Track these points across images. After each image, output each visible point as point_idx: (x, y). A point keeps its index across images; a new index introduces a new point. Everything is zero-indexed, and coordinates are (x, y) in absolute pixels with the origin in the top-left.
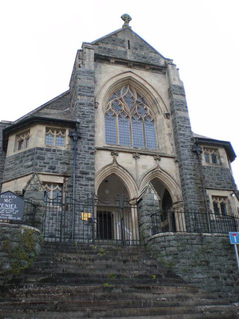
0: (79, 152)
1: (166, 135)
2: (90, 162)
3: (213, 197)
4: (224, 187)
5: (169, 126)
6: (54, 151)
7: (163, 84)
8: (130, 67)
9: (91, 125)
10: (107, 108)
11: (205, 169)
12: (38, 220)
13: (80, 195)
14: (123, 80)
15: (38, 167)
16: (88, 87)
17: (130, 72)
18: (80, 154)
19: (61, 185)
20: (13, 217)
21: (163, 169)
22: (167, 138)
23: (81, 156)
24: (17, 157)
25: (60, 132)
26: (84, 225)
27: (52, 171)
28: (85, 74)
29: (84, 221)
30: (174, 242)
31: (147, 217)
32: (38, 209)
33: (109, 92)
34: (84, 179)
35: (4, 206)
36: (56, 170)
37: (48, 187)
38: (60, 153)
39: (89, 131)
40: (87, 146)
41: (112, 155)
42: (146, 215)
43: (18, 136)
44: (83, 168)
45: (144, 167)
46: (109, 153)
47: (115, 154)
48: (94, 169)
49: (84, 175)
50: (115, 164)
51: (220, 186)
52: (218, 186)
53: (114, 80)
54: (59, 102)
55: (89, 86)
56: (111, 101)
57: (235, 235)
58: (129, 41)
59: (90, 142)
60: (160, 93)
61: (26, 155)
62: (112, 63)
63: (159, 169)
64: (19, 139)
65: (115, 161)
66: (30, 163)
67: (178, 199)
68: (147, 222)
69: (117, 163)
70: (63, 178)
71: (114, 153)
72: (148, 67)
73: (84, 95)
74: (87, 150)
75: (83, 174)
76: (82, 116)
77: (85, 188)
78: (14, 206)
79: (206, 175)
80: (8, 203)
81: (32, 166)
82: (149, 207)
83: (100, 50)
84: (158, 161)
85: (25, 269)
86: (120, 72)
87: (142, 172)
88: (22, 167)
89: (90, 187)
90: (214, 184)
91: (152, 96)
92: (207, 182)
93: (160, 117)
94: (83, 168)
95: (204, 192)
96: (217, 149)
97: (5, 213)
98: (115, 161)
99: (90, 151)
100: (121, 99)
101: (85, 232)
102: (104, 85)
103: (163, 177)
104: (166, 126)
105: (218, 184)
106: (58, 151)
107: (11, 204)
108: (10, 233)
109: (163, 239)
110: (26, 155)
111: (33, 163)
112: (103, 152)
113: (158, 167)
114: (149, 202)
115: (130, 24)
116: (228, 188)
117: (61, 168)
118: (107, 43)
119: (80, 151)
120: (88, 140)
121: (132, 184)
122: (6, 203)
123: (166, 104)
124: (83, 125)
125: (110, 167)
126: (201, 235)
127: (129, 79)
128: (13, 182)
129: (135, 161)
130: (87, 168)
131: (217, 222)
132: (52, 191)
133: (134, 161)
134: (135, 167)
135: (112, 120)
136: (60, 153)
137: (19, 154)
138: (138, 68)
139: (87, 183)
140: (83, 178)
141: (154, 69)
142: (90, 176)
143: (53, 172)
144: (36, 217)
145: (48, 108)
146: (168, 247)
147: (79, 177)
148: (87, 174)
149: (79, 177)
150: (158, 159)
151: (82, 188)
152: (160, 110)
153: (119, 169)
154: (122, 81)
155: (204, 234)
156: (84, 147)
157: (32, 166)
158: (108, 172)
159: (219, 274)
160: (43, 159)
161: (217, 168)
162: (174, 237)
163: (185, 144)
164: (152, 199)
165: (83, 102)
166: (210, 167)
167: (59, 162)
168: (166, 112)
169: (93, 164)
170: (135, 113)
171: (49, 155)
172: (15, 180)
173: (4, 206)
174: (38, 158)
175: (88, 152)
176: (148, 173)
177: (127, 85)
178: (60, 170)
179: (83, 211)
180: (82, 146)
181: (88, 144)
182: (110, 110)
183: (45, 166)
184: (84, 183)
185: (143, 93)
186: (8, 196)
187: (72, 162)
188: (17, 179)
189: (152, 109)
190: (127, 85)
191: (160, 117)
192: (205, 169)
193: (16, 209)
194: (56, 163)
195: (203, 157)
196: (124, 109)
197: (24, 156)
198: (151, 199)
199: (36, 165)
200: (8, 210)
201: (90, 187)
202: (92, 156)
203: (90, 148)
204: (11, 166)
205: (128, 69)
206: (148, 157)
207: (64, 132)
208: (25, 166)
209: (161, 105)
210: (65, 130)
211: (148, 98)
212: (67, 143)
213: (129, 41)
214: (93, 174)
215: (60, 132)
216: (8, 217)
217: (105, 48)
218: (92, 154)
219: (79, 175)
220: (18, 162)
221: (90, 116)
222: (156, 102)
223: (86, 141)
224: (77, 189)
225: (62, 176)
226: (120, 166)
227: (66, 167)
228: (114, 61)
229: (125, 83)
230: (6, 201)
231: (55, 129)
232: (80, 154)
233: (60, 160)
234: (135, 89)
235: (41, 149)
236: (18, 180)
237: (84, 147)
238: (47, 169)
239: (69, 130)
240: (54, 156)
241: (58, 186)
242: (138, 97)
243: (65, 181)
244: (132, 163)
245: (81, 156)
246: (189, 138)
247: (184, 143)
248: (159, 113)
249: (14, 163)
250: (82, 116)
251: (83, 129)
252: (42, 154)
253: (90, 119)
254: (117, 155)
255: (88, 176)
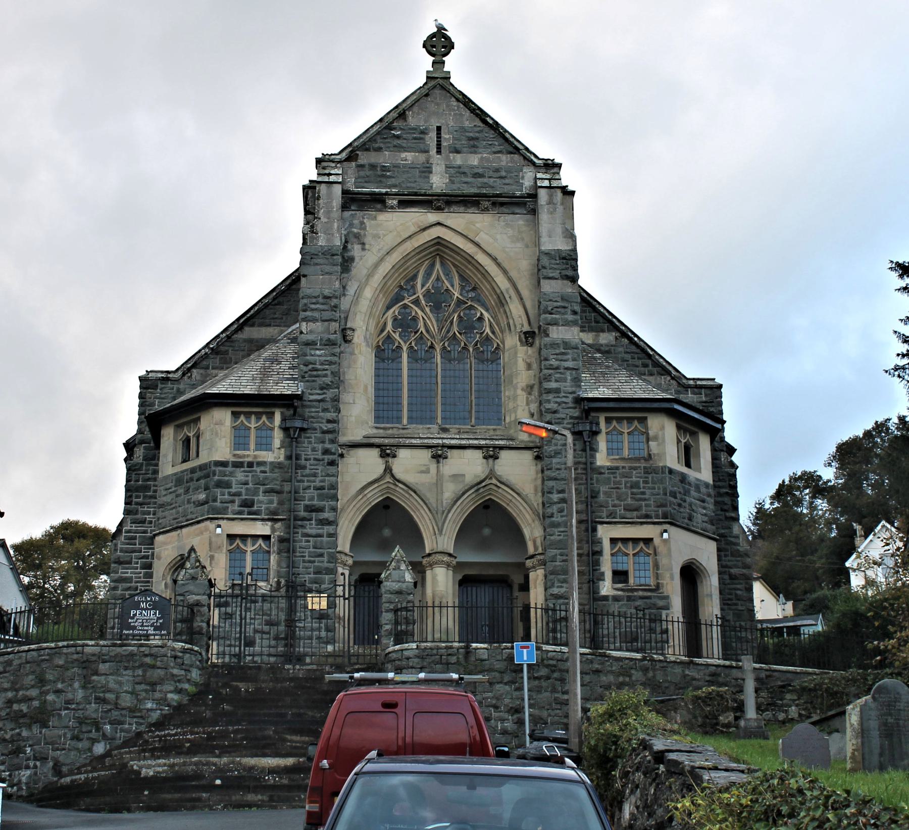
0: (303, 462)
1: (519, 392)
2: (326, 484)
3: (613, 541)
4: (647, 516)
5: (529, 367)
6: (250, 465)
7: (527, 246)
8: (439, 209)
9: (330, 394)
10: (382, 331)
11: (601, 473)
12: (198, 629)
13: (304, 556)
14: (420, 250)
15: (218, 504)
16: (326, 297)
17: (439, 224)
18: (304, 467)
19: (266, 538)
20: (154, 630)
21: (504, 480)
22: (522, 396)
23: (307, 471)
24: (179, 480)
25: (264, 418)
26: (312, 619)
27: (246, 509)
28: (319, 261)
29: (312, 610)
30: (416, 660)
31: (388, 614)
32: (199, 611)
33: (383, 287)
34: (313, 522)
35: (141, 613)
36: (255, 508)
37: (240, 544)
38: (263, 468)
39: (325, 410)
40: (320, 446)
41: (381, 456)
42: (387, 611)
43: (179, 427)
44: (310, 497)
45: (456, 477)
46: (375, 452)
47: (388, 455)
48: (335, 498)
49: (314, 514)
50: (388, 479)
51: (635, 513)
52: (628, 514)
53: (396, 257)
54: (279, 304)
55: (327, 292)
56: (392, 311)
57: (527, 647)
58: (439, 129)
59: (328, 437)
60: (513, 274)
61: (196, 476)
62: (392, 207)
63: (494, 481)
64: (181, 436)
65: (388, 470)
66: (202, 496)
67: (536, 548)
68: (386, 624)
69: (393, 476)
70: (269, 523)
71: (387, 452)
72: (486, 204)
73: (314, 320)
74: (320, 457)
75: (312, 511)
76: (310, 376)
77: (315, 542)
78: (155, 614)
79: (603, 489)
80: (146, 609)
81: (206, 502)
82: (392, 596)
83: (362, 173)
84: (491, 461)
85: (850, 667)
86: (413, 229)
87: (449, 491)
88: (189, 502)
89: (325, 539)
90: (620, 511)
91: (494, 284)
92: (601, 506)
93: (511, 341)
94: (312, 499)
95: (594, 530)
96: (646, 418)
97: (142, 626)
98: (388, 470)
99: (326, 457)
100: (417, 302)
101: (315, 633)
102: (370, 276)
103: (504, 497)
104: (521, 365)
105: (630, 510)
106: (260, 464)
107: (150, 610)
108: (151, 655)
109: (399, 655)
110: (196, 476)
111: (207, 497)
112: (361, 452)
113: (492, 474)
114: (396, 586)
115: (451, 63)
116: (657, 517)
117: (263, 501)
118: (379, 149)
119: (306, 460)
120: (324, 432)
121: (428, 521)
122: (143, 609)
123: (529, 305)
124: (312, 397)
125: (376, 485)
126: (467, 647)
127: (438, 244)
128: (174, 534)
129: (436, 465)
130: (321, 497)
131: (616, 599)
132: (249, 552)
133: (433, 467)
134: (435, 481)
135: (393, 360)
136: (263, 468)
137: (182, 472)
138: (462, 209)
139: (320, 531)
140: (311, 520)
141: (502, 204)
142: (326, 515)
143: (249, 513)
144: (195, 625)
145: (253, 325)
146: (405, 668)
147: (304, 519)
148: (320, 510)
149: (304, 519)
150: (491, 457)
151: (309, 541)
152: (511, 322)
153: (398, 489)
154: (419, 253)
155: (474, 645)
156: (314, 450)
157: (206, 502)
158: (374, 497)
159: (491, 714)
160: (228, 485)
161: (635, 468)
162: (417, 651)
163: (558, 416)
164: (402, 580)
165: (311, 337)
166: (617, 468)
167: (262, 488)
168: (526, 328)
169: (334, 487)
170: (451, 334)
171: (240, 475)
172: (179, 531)
173: (141, 613)
174: (219, 485)
175: (323, 460)
176: (463, 494)
177: (435, 257)
178: (264, 507)
179: (310, 591)
180: (310, 448)
181: (323, 442)
182: (389, 337)
183: (233, 502)
184: (313, 532)
185: (476, 278)
186: (146, 598)
187: (287, 487)
188: (182, 527)
189: (495, 317)
190: (435, 257)
191: (511, 341)
192: (601, 473)
193: (158, 618)
194: (256, 493)
195: (602, 443)
196: (422, 329)
197: (192, 479)
198: (399, 581)
199: (215, 500)
200: (147, 620)
201: (325, 539)
202: (332, 470)
203: (326, 452)
204: (168, 499)
205: (433, 217)
206: (469, 453)
207: (271, 416)
208: (194, 503)
209: (515, 308)
210: (273, 413)
211: (485, 287)
212: (277, 443)
213: (439, 129)
214: (334, 509)
215: (264, 418)
216: (147, 631)
217: (373, 167)
218: (332, 463)
219: (302, 514)
220: (181, 491)
221: (329, 372)
222: (503, 301)
223: (318, 435)
224: (298, 545)
225: (269, 520)
226: (399, 481)
227: (275, 498)
228: (395, 202)
229: (431, 253)
230: (143, 605)
231: (251, 413)
232: (304, 467)
233: (264, 485)
234: (455, 265)
235: (224, 464)
236: (184, 530)
237: (314, 450)
238: (236, 507)
239: (282, 413)
240: (250, 478)
241: (260, 541)
242: (462, 288)
243: (273, 530)
244: (427, 471)
245: (307, 471)
246: (570, 399)
247: (555, 412)
248: (510, 329)
249: (174, 492)
250: (310, 376)
251: (310, 407)
252: (226, 475)
253: (328, 380)
254: (394, 456)
255: (305, 531)
